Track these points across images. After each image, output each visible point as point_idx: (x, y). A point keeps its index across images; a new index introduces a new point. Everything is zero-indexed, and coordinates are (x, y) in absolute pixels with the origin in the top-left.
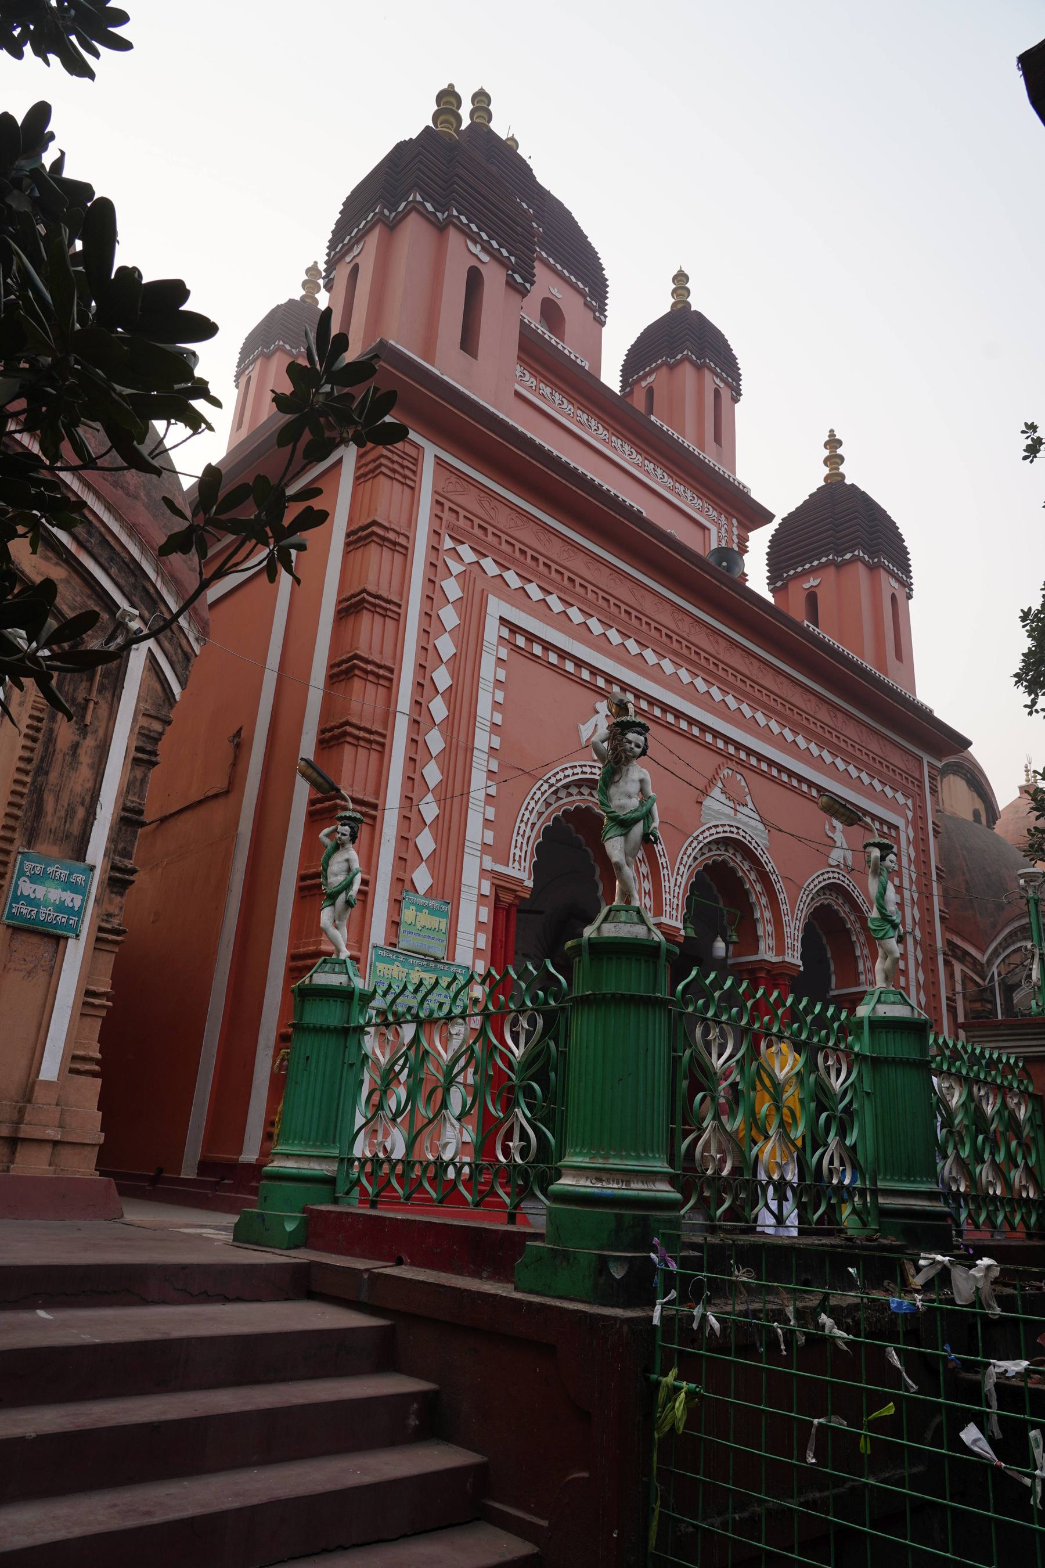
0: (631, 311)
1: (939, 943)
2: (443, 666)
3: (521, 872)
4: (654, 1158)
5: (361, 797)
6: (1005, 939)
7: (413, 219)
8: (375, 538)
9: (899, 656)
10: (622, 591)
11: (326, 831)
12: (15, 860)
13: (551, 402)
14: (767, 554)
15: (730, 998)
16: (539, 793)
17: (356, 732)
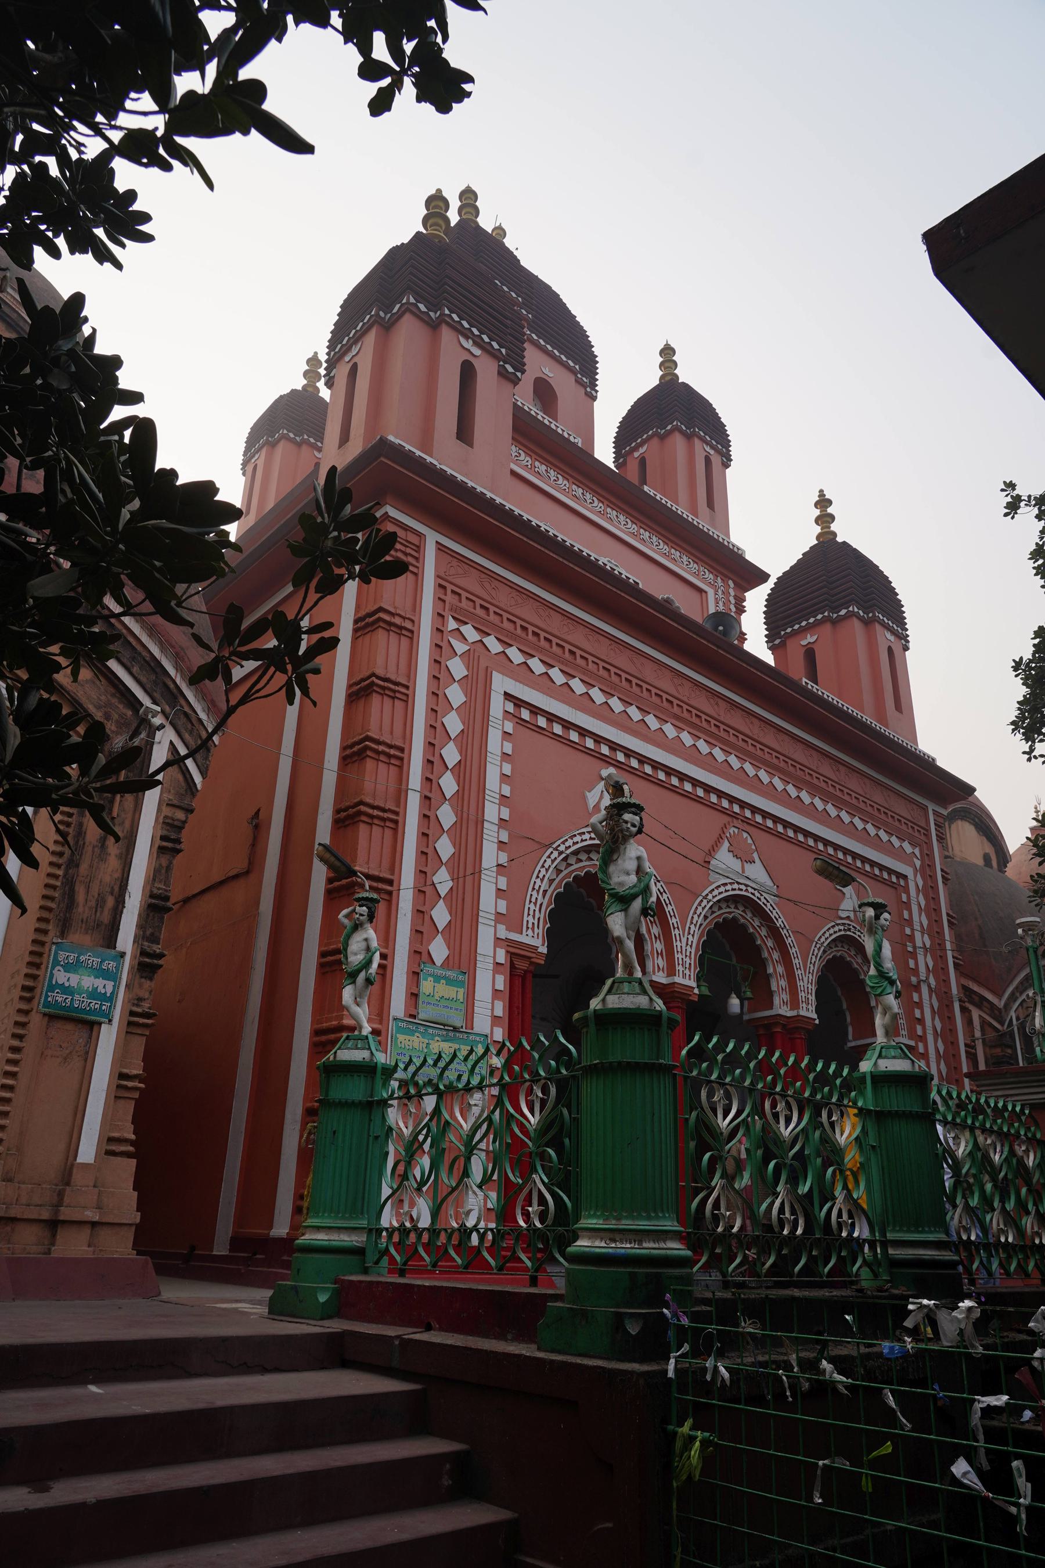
0: (621, 384)
1: (954, 990)
2: (451, 743)
3: (534, 938)
4: (664, 1217)
5: (376, 873)
6: (1021, 983)
7: (408, 320)
8: (381, 624)
9: (898, 707)
10: (622, 660)
11: (345, 912)
12: (50, 950)
13: (546, 479)
14: (764, 613)
15: (733, 1060)
16: (549, 861)
17: (370, 811)
